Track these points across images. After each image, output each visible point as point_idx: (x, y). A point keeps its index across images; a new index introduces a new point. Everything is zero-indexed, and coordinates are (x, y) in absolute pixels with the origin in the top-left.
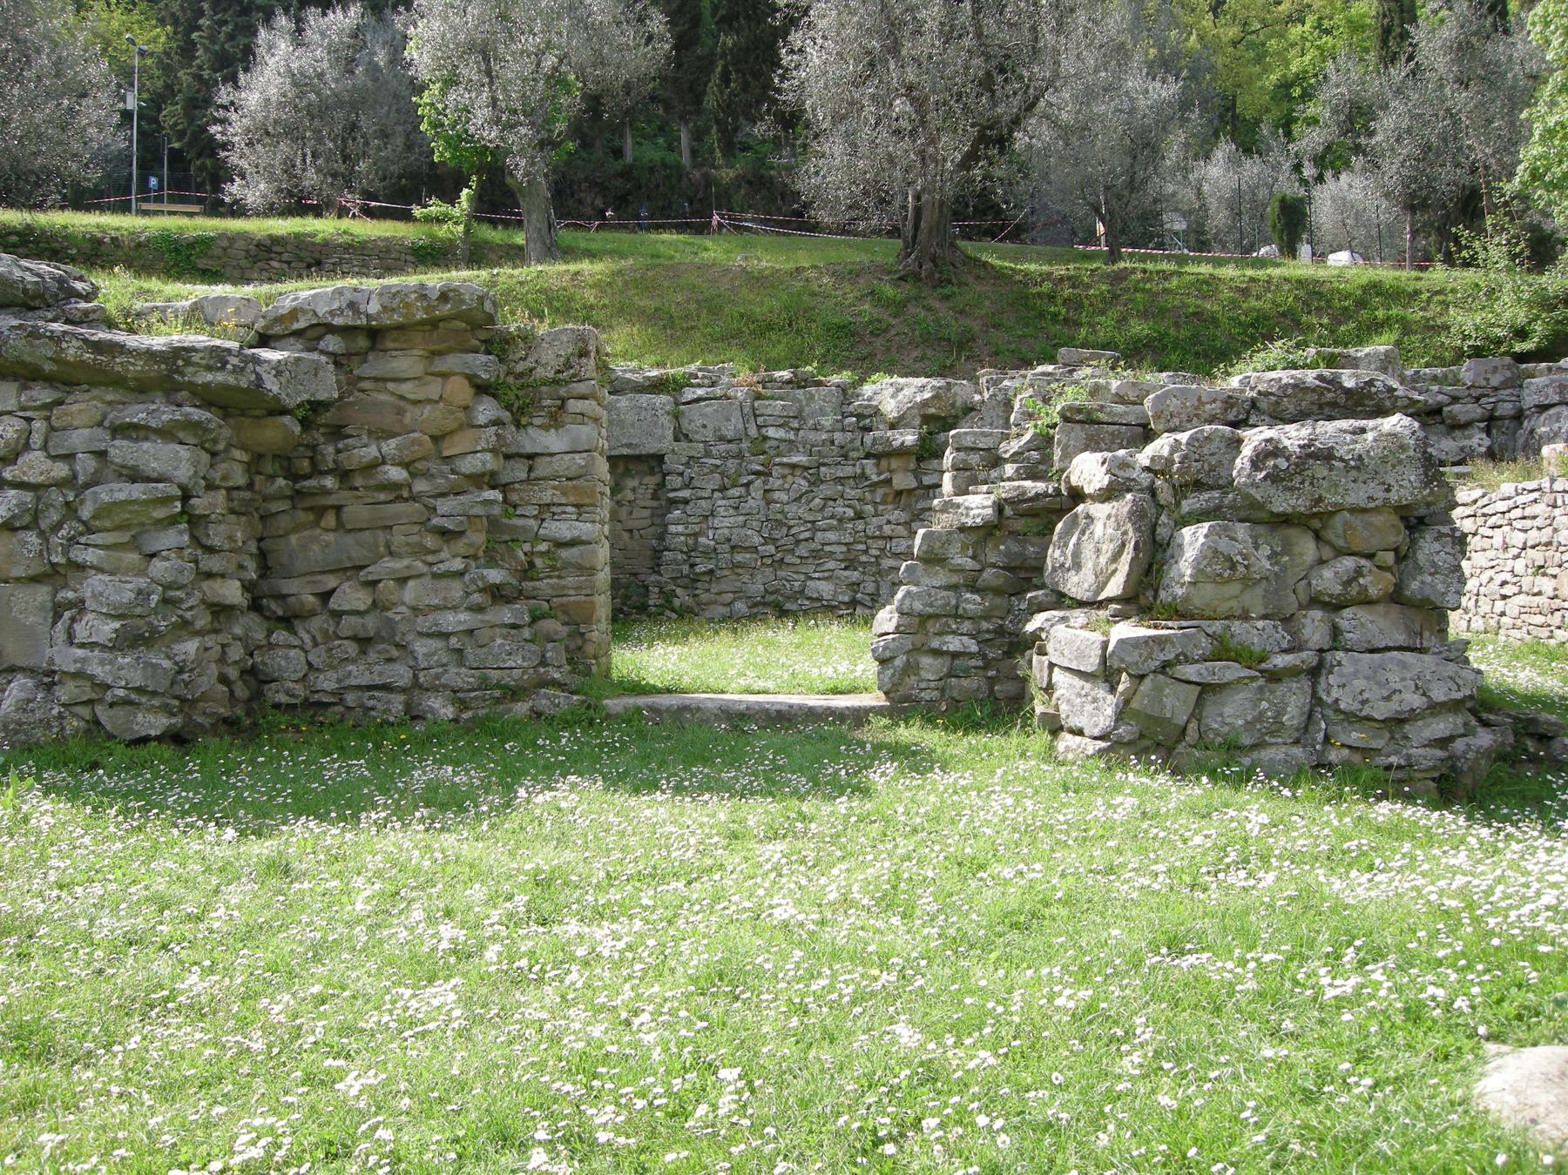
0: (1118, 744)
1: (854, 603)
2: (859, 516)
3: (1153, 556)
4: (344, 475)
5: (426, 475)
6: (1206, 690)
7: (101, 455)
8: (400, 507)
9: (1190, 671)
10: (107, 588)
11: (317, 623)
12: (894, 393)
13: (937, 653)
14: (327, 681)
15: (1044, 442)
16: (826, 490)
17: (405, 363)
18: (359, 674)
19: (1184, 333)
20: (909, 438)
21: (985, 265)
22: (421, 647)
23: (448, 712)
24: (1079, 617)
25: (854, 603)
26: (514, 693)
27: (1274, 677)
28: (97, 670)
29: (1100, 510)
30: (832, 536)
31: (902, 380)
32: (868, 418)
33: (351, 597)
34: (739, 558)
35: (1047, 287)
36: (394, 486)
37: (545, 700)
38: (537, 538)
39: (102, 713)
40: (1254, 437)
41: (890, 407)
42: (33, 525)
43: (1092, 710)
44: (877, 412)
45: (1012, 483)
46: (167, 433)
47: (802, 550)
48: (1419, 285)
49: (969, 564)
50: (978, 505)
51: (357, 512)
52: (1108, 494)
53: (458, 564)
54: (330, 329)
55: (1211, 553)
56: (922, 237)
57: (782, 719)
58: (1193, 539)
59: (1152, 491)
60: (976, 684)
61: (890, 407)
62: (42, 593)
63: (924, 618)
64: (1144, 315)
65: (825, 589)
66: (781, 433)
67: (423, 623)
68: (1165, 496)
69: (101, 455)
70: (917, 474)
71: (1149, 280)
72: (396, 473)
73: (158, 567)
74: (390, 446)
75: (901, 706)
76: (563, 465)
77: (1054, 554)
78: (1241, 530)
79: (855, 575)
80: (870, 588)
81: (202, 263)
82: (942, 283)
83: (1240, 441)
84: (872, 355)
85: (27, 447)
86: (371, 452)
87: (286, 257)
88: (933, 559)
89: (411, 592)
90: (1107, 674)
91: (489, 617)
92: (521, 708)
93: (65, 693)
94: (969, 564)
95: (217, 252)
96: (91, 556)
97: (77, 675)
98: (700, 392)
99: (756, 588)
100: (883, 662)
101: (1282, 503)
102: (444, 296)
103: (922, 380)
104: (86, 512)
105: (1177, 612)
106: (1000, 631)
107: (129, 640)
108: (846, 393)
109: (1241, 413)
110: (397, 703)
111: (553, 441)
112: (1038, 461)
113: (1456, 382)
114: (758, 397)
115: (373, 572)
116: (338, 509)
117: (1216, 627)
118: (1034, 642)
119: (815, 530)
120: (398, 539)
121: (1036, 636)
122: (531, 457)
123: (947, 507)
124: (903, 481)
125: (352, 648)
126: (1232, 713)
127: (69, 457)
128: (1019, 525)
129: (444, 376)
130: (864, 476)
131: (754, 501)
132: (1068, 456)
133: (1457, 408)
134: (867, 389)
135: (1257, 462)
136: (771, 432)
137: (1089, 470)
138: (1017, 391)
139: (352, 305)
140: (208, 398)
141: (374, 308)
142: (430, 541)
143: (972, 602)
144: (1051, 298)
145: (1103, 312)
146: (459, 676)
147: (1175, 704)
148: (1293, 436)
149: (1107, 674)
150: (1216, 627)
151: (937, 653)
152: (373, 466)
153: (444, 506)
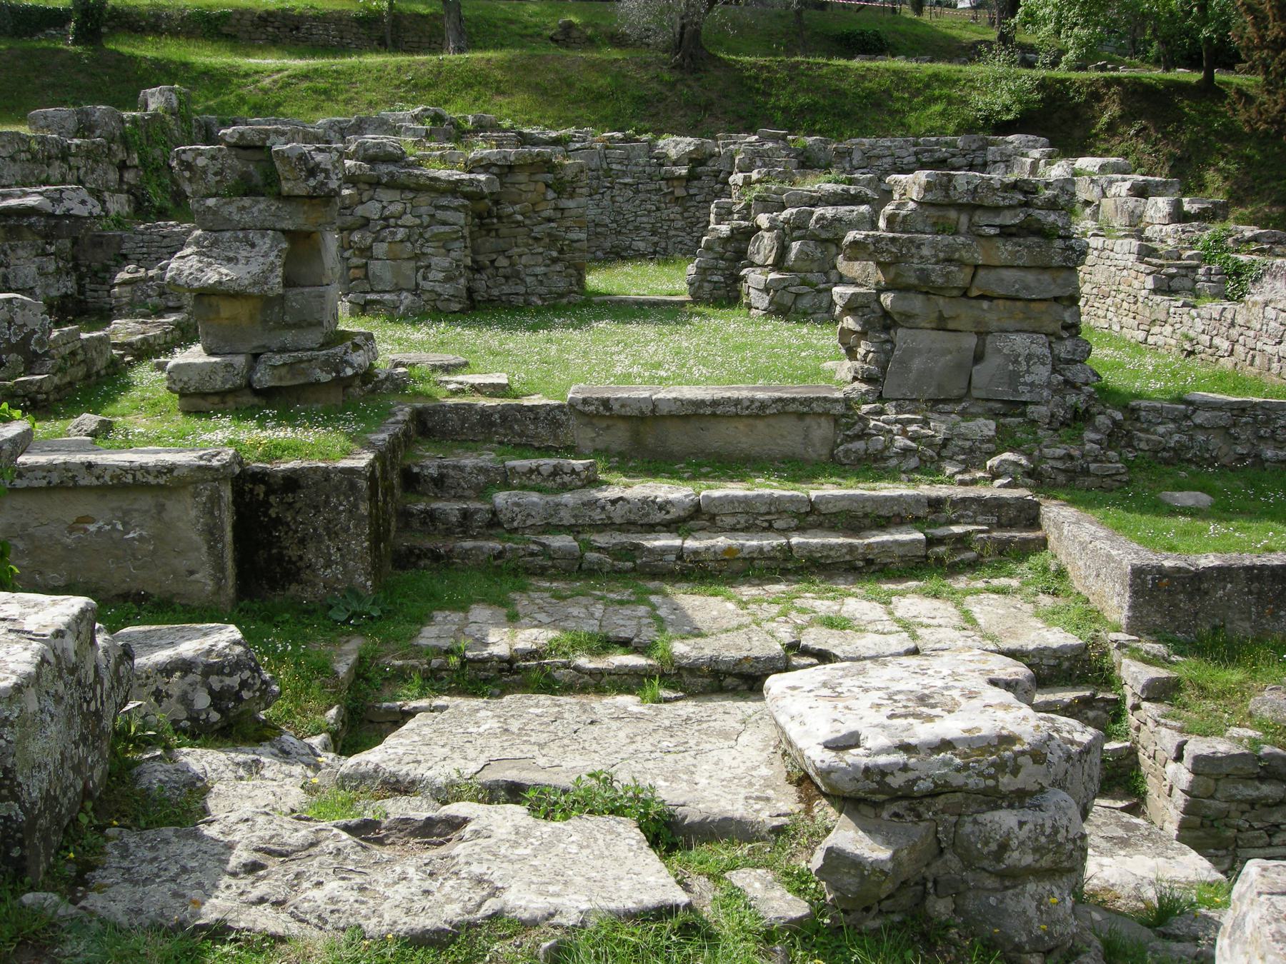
0: (770, 312)
1: (655, 252)
2: (658, 209)
3: (783, 251)
4: (499, 218)
5: (529, 218)
6: (798, 295)
7: (432, 216)
8: (520, 229)
9: (793, 289)
10: (440, 262)
11: (489, 271)
12: (675, 145)
13: (710, 282)
14: (495, 292)
15: (748, 207)
16: (642, 196)
17: (522, 177)
18: (506, 289)
19: (827, 102)
20: (683, 171)
21: (720, 59)
22: (528, 279)
23: (540, 302)
24: (758, 270)
25: (655, 252)
26: (562, 296)
27: (819, 291)
28: (439, 290)
29: (767, 235)
30: (645, 219)
31: (679, 139)
32: (662, 159)
33: (502, 262)
34: (598, 230)
35: (753, 72)
36: (518, 222)
37: (573, 297)
38: (565, 239)
39: (439, 304)
40: (819, 211)
41: (673, 153)
42: (408, 240)
43: (761, 301)
44: (666, 156)
45: (736, 222)
46: (456, 209)
47: (630, 227)
48: (961, 75)
49: (721, 250)
50: (724, 229)
51: (504, 231)
52: (769, 230)
53: (541, 250)
54: (495, 165)
55: (801, 251)
56: (685, 43)
57: (655, 304)
58: (795, 246)
59: (783, 229)
60: (721, 291)
61: (673, 153)
62: (412, 264)
63: (705, 269)
64: (807, 91)
65: (641, 245)
66: (619, 167)
67: (529, 271)
68: (787, 231)
69: (432, 216)
70: (687, 188)
71: (810, 69)
72: (520, 218)
73: (453, 254)
74: (517, 207)
75: (697, 299)
76: (573, 212)
77: (751, 248)
78: (811, 243)
79: (656, 239)
80: (663, 245)
81: (225, 30)
82: (696, 70)
83: (813, 213)
84: (658, 114)
85: (405, 213)
86: (510, 210)
87: (276, 24)
88: (709, 248)
89: (524, 260)
90: (766, 290)
91: (552, 268)
92: (565, 301)
93: (425, 297)
94: (721, 250)
95: (234, 22)
96: (429, 251)
97: (432, 291)
98: (578, 145)
99: (608, 245)
100: (691, 284)
101: (824, 235)
102: (538, 154)
103: (689, 139)
104: (427, 236)
105: (790, 270)
106: (732, 274)
107: (448, 279)
108: (651, 146)
109: (815, 201)
110: (521, 299)
111: (571, 204)
112: (746, 214)
113: (955, 147)
114: (607, 148)
115: (510, 253)
116: (497, 230)
117: (802, 275)
118: (743, 278)
119: (636, 216)
120: (519, 241)
121: (744, 276)
122: (563, 209)
123: (714, 229)
124: (680, 192)
125: (503, 280)
126: (805, 303)
127: (420, 217)
128: (739, 237)
129: (536, 182)
130: (660, 190)
131: (606, 202)
132: (757, 213)
133: (954, 159)
134: (661, 143)
135: (817, 222)
136: (614, 166)
137: (763, 220)
138: (737, 152)
139: (505, 157)
140: (466, 196)
141: (512, 158)
142: (531, 242)
143: (722, 264)
144: (756, 79)
145: (784, 88)
146: (543, 290)
147: (788, 300)
148: (829, 211)
149: (766, 290)
150: (802, 275)
151: (710, 282)
152: (510, 216)
153: (536, 229)
